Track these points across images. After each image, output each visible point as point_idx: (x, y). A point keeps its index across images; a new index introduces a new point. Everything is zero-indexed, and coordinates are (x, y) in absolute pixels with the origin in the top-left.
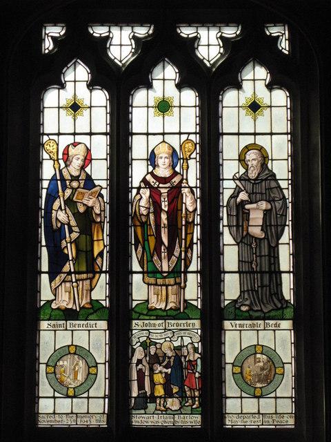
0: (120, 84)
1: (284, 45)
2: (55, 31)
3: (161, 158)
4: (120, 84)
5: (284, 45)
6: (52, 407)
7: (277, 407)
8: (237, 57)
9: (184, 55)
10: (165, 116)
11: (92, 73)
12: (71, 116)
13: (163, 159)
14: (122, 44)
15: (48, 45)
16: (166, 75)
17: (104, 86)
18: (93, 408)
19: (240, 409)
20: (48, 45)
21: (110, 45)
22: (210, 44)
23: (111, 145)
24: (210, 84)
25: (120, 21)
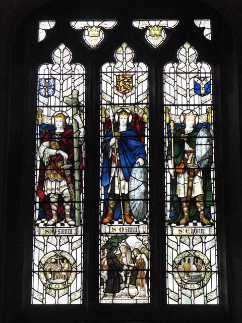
0: (92, 60)
1: (207, 33)
2: (45, 26)
3: (122, 118)
4: (92, 60)
5: (207, 33)
6: (42, 293)
7: (209, 293)
8: (174, 41)
9: (138, 41)
10: (124, 84)
11: (84, 41)
12: (60, 84)
13: (123, 119)
14: (93, 33)
15: (42, 36)
16: (124, 54)
17: (83, 63)
18: (71, 293)
19: (178, 293)
20: (42, 36)
21: (70, 54)
22: (155, 33)
23: (89, 46)
24: (157, 60)
25: (33, 149)
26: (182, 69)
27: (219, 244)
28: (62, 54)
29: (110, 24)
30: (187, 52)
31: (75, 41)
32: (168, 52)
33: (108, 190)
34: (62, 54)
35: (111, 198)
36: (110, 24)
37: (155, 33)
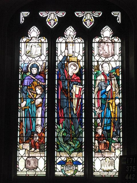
0: (51, 35)
2: (24, 14)
4: (51, 35)
9: (78, 25)
12: (32, 51)
20: (22, 21)
24: (88, 36)
26: (105, 61)
27: (50, 167)
28: (34, 32)
29: (61, 14)
30: (107, 32)
31: (42, 24)
32: (96, 31)
33: (27, 95)
34: (34, 32)
35: (100, 119)
36: (61, 14)
37: (88, 19)
